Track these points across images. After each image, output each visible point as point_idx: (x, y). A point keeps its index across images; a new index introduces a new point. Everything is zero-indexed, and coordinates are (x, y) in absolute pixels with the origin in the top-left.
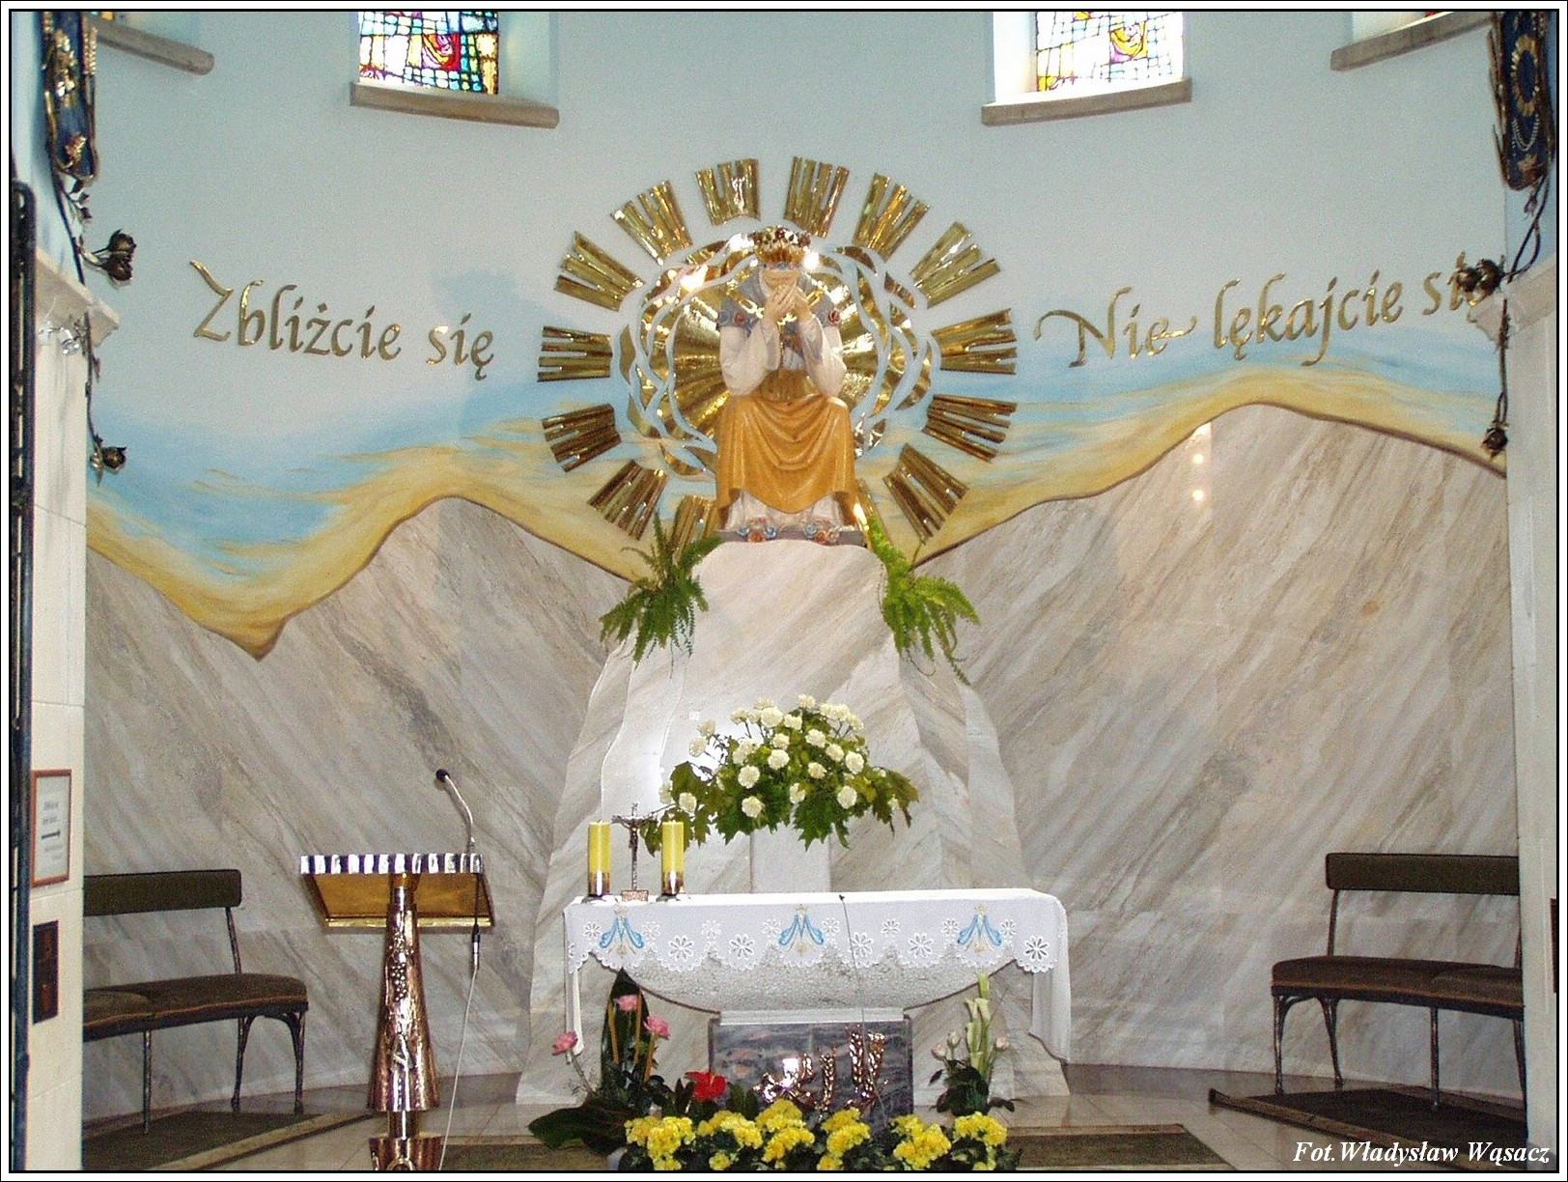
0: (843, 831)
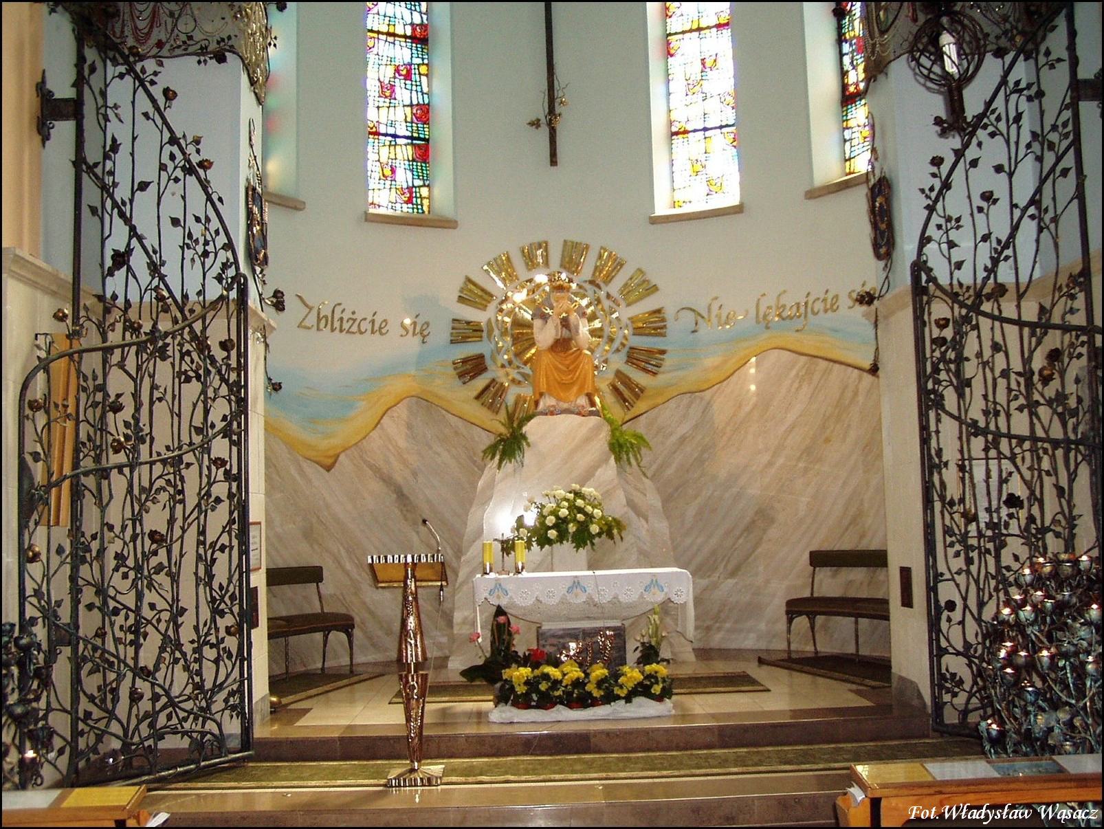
0: (593, 544)
